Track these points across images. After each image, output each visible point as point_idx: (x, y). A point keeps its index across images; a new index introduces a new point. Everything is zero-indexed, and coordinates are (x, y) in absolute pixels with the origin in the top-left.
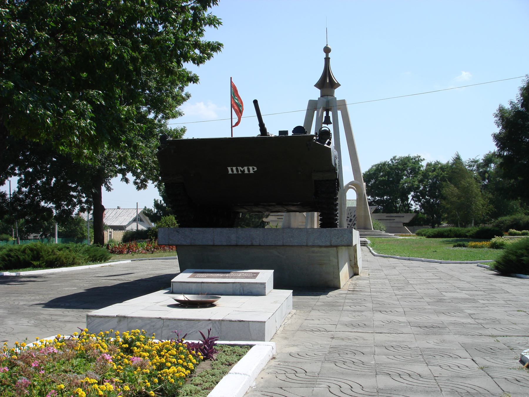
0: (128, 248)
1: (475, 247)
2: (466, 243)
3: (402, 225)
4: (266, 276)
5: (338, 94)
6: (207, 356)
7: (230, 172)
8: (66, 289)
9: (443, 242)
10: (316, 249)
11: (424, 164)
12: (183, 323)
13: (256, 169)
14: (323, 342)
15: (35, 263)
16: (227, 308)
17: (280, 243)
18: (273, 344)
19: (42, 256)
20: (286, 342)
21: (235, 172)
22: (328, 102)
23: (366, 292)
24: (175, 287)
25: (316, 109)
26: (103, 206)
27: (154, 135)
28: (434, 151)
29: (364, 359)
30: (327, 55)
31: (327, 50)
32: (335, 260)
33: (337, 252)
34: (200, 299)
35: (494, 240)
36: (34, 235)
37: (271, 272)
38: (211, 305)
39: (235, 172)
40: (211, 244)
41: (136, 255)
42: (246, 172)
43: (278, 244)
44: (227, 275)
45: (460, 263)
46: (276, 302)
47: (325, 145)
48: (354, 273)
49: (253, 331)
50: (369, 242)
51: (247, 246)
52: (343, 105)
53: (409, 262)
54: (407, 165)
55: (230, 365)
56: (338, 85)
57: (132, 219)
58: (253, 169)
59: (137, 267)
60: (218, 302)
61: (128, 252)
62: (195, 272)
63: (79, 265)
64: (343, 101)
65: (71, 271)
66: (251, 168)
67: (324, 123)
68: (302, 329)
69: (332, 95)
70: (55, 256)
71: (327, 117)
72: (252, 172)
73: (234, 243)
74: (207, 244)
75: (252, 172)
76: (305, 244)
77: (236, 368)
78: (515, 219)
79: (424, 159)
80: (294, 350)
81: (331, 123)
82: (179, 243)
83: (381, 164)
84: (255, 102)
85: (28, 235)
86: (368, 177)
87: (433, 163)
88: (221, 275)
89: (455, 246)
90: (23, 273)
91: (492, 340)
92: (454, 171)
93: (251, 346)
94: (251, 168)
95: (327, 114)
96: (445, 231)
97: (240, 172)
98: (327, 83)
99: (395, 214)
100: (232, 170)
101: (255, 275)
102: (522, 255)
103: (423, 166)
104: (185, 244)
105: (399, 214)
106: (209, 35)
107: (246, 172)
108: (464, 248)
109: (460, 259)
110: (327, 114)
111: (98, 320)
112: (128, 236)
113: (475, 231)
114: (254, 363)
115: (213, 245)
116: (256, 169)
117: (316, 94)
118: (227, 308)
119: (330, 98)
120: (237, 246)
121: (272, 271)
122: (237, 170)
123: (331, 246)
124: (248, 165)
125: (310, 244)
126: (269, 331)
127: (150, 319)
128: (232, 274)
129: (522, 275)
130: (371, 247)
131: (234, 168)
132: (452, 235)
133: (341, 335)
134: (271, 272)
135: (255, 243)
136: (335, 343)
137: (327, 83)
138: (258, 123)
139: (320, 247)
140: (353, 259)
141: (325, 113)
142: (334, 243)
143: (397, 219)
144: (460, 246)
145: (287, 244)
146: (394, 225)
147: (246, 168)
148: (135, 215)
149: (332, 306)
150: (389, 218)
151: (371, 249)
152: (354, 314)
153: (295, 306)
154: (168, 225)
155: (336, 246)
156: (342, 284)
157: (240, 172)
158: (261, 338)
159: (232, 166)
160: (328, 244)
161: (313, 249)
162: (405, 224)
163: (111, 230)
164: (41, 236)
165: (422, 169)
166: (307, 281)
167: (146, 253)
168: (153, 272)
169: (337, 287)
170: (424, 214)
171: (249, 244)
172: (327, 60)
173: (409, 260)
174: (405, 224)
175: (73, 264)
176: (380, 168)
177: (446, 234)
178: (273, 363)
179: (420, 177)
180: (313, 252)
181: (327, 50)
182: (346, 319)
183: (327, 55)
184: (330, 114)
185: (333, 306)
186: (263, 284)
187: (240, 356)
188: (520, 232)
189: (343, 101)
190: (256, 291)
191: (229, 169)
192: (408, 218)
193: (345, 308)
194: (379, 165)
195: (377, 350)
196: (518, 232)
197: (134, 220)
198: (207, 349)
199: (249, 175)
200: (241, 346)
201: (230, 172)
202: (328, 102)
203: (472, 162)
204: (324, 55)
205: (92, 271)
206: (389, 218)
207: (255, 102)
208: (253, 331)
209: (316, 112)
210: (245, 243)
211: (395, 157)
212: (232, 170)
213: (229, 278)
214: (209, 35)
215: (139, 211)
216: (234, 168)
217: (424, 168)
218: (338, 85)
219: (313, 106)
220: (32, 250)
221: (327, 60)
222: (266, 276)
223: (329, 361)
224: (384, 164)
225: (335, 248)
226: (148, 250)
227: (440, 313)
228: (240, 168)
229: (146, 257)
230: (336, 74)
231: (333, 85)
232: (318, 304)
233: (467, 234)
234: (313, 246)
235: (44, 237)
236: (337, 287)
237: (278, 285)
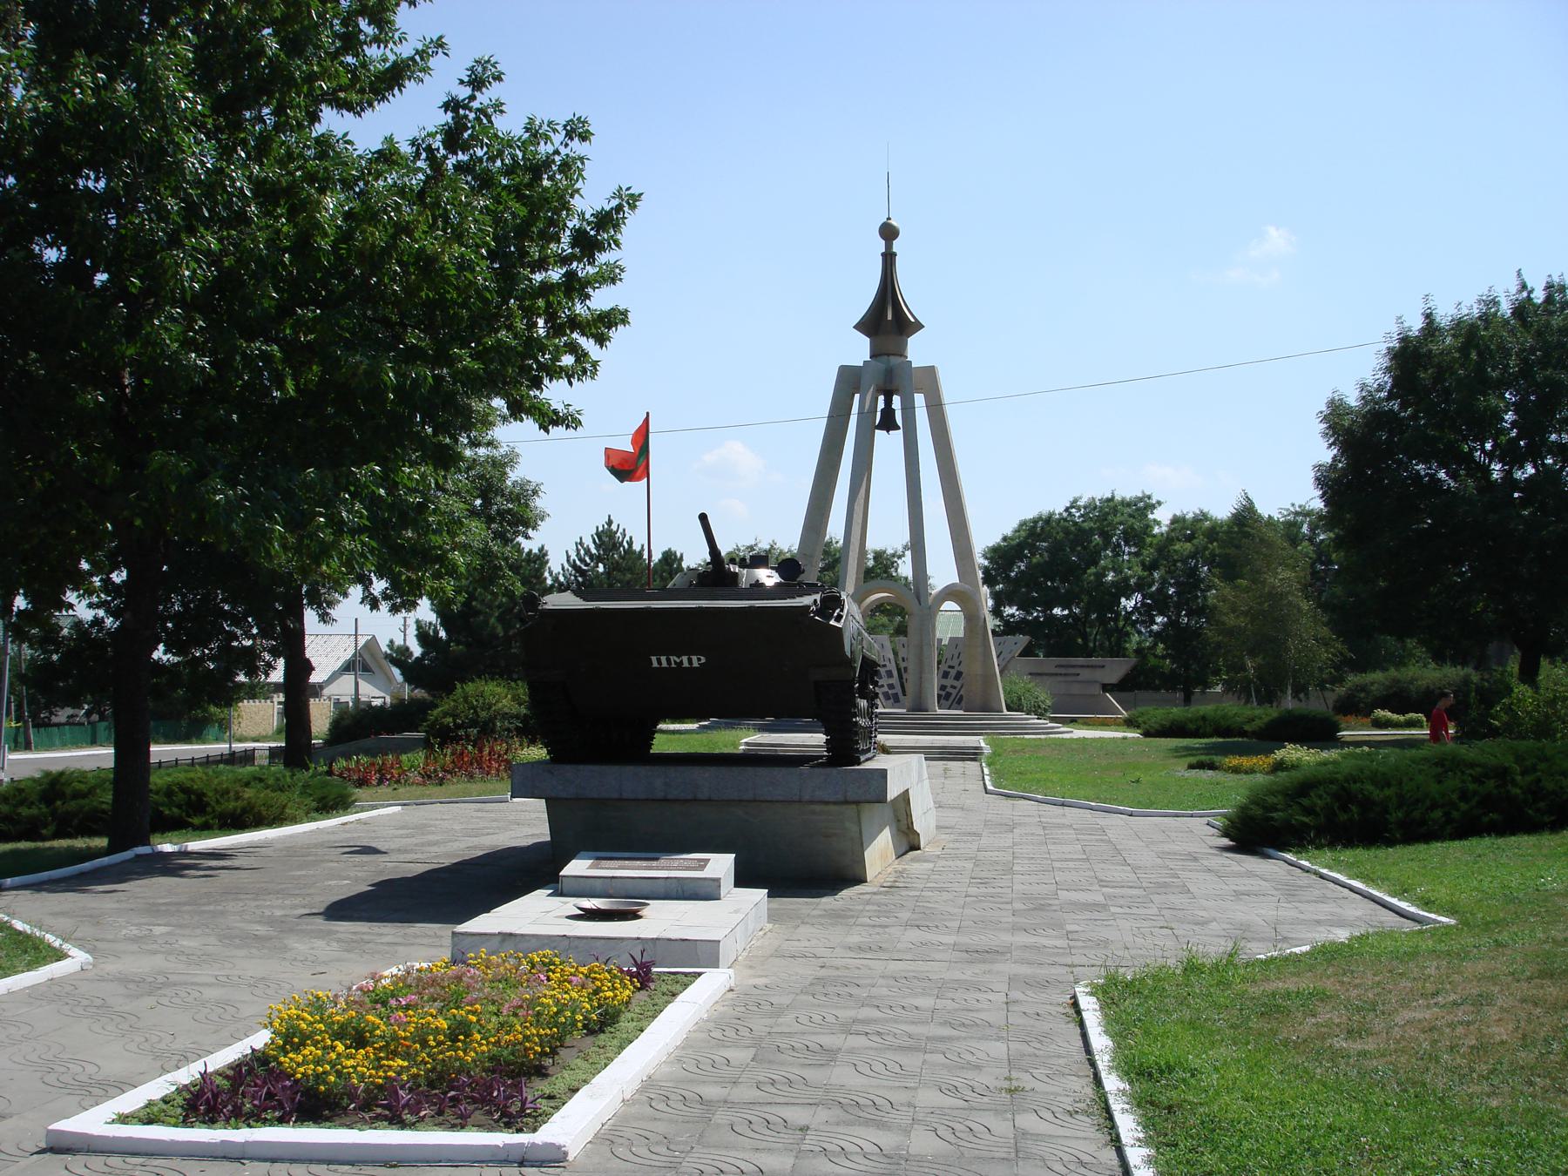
0: (379, 771)
1: (1236, 770)
2: (1217, 759)
3: (1098, 690)
4: (721, 865)
5: (918, 351)
6: (643, 987)
7: (655, 664)
8: (332, 883)
9: (1176, 750)
10: (817, 808)
11: (1162, 517)
12: (599, 943)
13: (703, 660)
14: (806, 971)
15: (196, 821)
16: (662, 920)
18: (731, 971)
19: (208, 804)
20: (751, 972)
21: (665, 664)
22: (889, 374)
23: (915, 889)
24: (566, 885)
26: (308, 661)
28: (1189, 485)
29: (855, 991)
30: (889, 246)
31: (889, 232)
32: (855, 828)
33: (859, 813)
34: (615, 907)
35: (1279, 754)
36: (69, 711)
37: (730, 858)
38: (633, 915)
39: (665, 664)
40: (616, 796)
41: (401, 790)
42: (686, 664)
44: (654, 863)
45: (1177, 816)
46: (736, 912)
47: (832, 622)
48: (909, 842)
49: (702, 954)
50: (987, 750)
51: (686, 801)
52: (928, 380)
53: (1059, 810)
54: (1114, 524)
55: (674, 995)
56: (918, 326)
57: (339, 664)
59: (425, 826)
60: (644, 912)
61: (380, 782)
62: (598, 858)
63: (294, 820)
64: (930, 372)
65: (291, 836)
66: (694, 658)
67: (880, 427)
68: (778, 954)
69: (901, 353)
70: (239, 804)
71: (888, 412)
72: (696, 664)
73: (660, 795)
75: (696, 664)
77: (680, 997)
78: (1396, 681)
79: (1159, 503)
80: (761, 981)
81: (897, 428)
83: (1040, 518)
84: (703, 518)
85: (51, 713)
86: (1002, 556)
87: (1190, 516)
88: (644, 863)
89: (1191, 767)
90: (195, 845)
91: (1064, 970)
92: (1239, 540)
93: (700, 974)
94: (694, 658)
95: (888, 402)
96: (1191, 721)
98: (887, 321)
100: (658, 661)
101: (702, 864)
102: (1274, 808)
103: (1158, 523)
104: (564, 795)
106: (601, 299)
107: (686, 664)
108: (1210, 772)
109: (1179, 805)
110: (888, 402)
111: (470, 939)
112: (347, 722)
113: (1266, 719)
114: (705, 992)
115: (620, 800)
116: (703, 660)
117: (858, 350)
118: (662, 920)
119: (894, 360)
120: (665, 800)
122: (669, 661)
123: (846, 802)
124: (689, 654)
125: (807, 797)
126: (727, 952)
127: (549, 937)
128: (663, 862)
129: (1271, 851)
130: (989, 765)
131: (663, 659)
132: (1209, 729)
133: (839, 962)
134: (730, 858)
136: (823, 972)
137: (887, 321)
139: (827, 803)
140: (903, 817)
141: (881, 398)
142: (851, 796)
143: (1085, 674)
144: (1201, 766)
146: (1076, 689)
147: (685, 659)
148: (351, 652)
149: (837, 916)
150: (1063, 671)
151: (986, 771)
152: (871, 931)
153: (773, 917)
154: (474, 708)
155: (857, 803)
156: (870, 875)
158: (714, 963)
159: (658, 654)
160: (840, 797)
162: (1106, 688)
164: (88, 714)
165: (1156, 530)
166: (803, 866)
167: (424, 784)
168: (475, 841)
169: (861, 880)
170: (1164, 657)
171: (690, 797)
172: (889, 258)
173: (1063, 805)
174: (1106, 688)
175: (278, 820)
176: (1036, 532)
177: (1192, 726)
178: (730, 995)
179: (1149, 554)
181: (889, 232)
182: (854, 939)
183: (889, 246)
185: (839, 916)
186: (718, 880)
187: (686, 986)
188: (1402, 718)
189: (930, 372)
190: (705, 892)
191: (654, 659)
192: (1115, 670)
193: (860, 920)
194: (1035, 521)
195: (881, 981)
196: (1395, 716)
197: (348, 667)
198: (643, 976)
199: (691, 669)
200: (686, 974)
201: (655, 664)
202: (889, 374)
203: (1297, 514)
204: (881, 245)
205: (326, 838)
206: (1063, 671)
207: (703, 518)
208: (702, 954)
209: (857, 396)
211: (1075, 501)
212: (658, 661)
213: (658, 869)
214: (601, 299)
215: (360, 645)
216: (663, 659)
217: (1164, 529)
218: (918, 326)
219: (849, 381)
220: (186, 790)
221: (889, 258)
222: (721, 865)
223: (807, 993)
224: (1048, 520)
226: (429, 777)
227: (1019, 929)
229: (429, 796)
230: (913, 297)
232: (815, 913)
233: (1247, 728)
234: (812, 802)
235: (95, 717)
236: (861, 880)
237: (744, 878)
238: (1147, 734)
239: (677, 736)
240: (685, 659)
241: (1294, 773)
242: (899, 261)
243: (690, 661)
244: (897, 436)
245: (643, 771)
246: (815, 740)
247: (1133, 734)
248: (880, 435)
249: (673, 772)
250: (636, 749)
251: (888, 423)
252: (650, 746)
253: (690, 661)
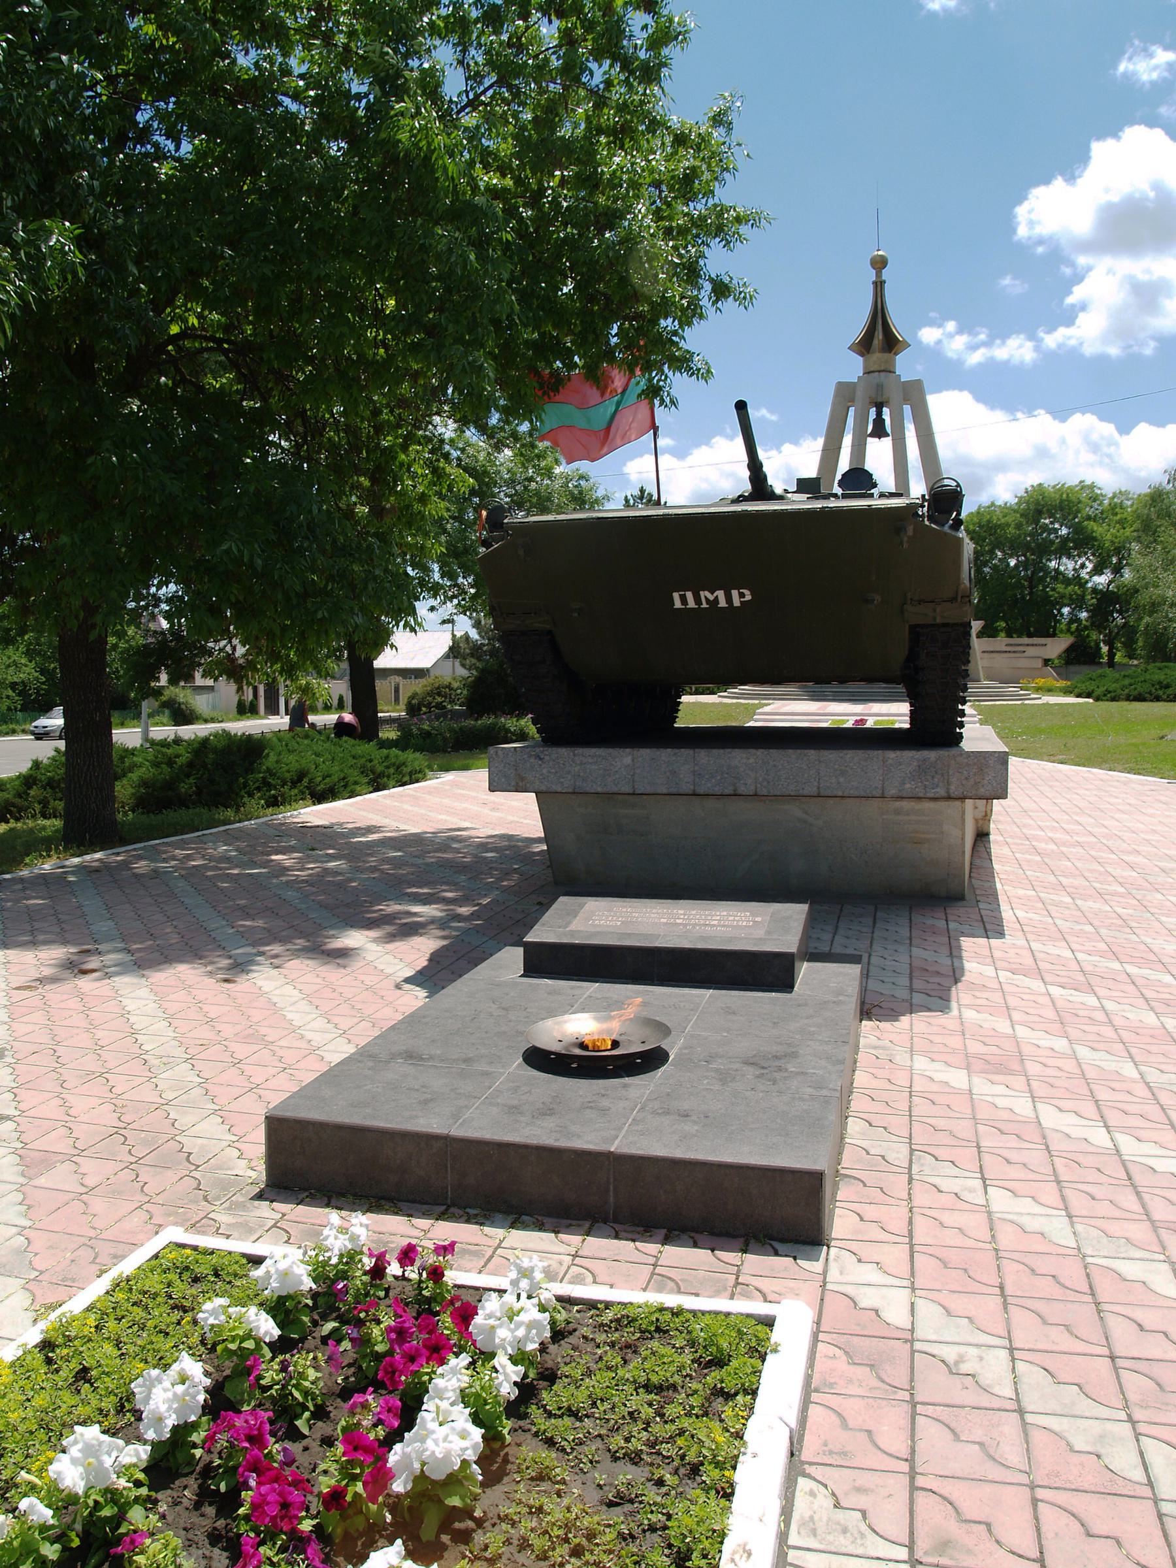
5: (905, 366)
7: (678, 604)
10: (906, 805)
13: (748, 597)
17: (811, 790)
22: (880, 387)
25: (852, 400)
27: (655, 13)
30: (879, 274)
31: (879, 264)
39: (691, 604)
40: (626, 789)
42: (723, 603)
43: (806, 792)
58: (742, 595)
67: (871, 435)
71: (879, 422)
72: (736, 602)
73: (686, 788)
74: (615, 789)
76: (878, 793)
82: (544, 788)
95: (879, 414)
97: (705, 605)
99: (1026, 640)
105: (1035, 640)
107: (723, 603)
116: (748, 597)
117: (853, 368)
121: (805, 907)
122: (698, 600)
123: (949, 798)
135: (742, 790)
138: (744, 457)
142: (954, 790)
143: (1031, 651)
145: (829, 793)
150: (1008, 649)
157: (705, 605)
161: (898, 804)
163: (398, 679)
172: (879, 286)
180: (898, 812)
181: (879, 264)
183: (879, 274)
184: (886, 414)
191: (676, 596)
204: (872, 275)
207: (741, 406)
210: (717, 790)
219: (845, 395)
221: (879, 286)
225: (958, 803)
228: (704, 594)
231: (892, 344)
238: (1097, 699)
239: (699, 707)
240: (720, 594)
241: (423, 681)
242: (888, 288)
243: (729, 599)
244: (886, 444)
245: (665, 755)
246: (894, 713)
247: (1091, 700)
248: (871, 441)
249: (706, 758)
250: (652, 724)
251: (879, 431)
252: (674, 719)
253: (729, 599)
